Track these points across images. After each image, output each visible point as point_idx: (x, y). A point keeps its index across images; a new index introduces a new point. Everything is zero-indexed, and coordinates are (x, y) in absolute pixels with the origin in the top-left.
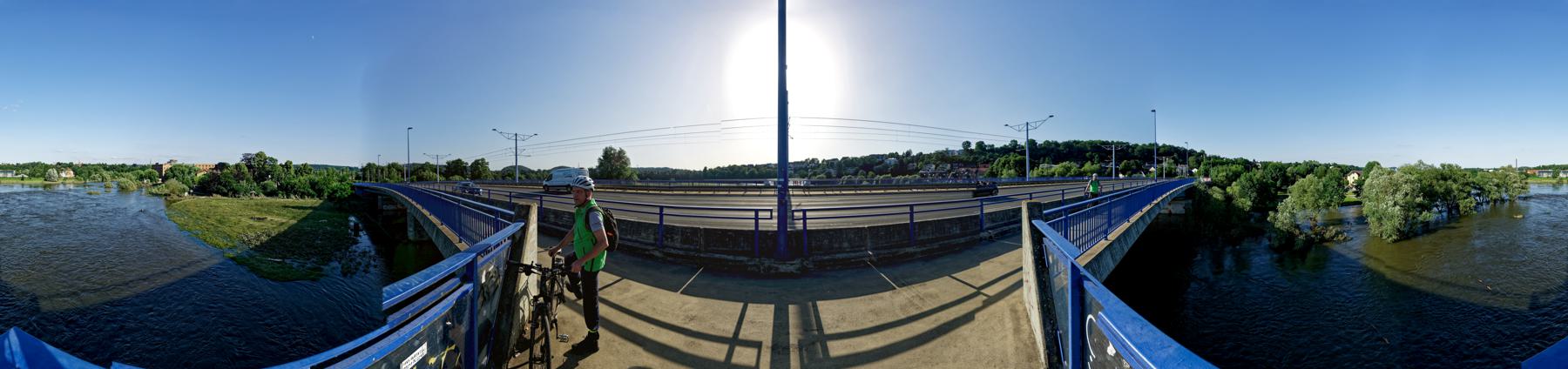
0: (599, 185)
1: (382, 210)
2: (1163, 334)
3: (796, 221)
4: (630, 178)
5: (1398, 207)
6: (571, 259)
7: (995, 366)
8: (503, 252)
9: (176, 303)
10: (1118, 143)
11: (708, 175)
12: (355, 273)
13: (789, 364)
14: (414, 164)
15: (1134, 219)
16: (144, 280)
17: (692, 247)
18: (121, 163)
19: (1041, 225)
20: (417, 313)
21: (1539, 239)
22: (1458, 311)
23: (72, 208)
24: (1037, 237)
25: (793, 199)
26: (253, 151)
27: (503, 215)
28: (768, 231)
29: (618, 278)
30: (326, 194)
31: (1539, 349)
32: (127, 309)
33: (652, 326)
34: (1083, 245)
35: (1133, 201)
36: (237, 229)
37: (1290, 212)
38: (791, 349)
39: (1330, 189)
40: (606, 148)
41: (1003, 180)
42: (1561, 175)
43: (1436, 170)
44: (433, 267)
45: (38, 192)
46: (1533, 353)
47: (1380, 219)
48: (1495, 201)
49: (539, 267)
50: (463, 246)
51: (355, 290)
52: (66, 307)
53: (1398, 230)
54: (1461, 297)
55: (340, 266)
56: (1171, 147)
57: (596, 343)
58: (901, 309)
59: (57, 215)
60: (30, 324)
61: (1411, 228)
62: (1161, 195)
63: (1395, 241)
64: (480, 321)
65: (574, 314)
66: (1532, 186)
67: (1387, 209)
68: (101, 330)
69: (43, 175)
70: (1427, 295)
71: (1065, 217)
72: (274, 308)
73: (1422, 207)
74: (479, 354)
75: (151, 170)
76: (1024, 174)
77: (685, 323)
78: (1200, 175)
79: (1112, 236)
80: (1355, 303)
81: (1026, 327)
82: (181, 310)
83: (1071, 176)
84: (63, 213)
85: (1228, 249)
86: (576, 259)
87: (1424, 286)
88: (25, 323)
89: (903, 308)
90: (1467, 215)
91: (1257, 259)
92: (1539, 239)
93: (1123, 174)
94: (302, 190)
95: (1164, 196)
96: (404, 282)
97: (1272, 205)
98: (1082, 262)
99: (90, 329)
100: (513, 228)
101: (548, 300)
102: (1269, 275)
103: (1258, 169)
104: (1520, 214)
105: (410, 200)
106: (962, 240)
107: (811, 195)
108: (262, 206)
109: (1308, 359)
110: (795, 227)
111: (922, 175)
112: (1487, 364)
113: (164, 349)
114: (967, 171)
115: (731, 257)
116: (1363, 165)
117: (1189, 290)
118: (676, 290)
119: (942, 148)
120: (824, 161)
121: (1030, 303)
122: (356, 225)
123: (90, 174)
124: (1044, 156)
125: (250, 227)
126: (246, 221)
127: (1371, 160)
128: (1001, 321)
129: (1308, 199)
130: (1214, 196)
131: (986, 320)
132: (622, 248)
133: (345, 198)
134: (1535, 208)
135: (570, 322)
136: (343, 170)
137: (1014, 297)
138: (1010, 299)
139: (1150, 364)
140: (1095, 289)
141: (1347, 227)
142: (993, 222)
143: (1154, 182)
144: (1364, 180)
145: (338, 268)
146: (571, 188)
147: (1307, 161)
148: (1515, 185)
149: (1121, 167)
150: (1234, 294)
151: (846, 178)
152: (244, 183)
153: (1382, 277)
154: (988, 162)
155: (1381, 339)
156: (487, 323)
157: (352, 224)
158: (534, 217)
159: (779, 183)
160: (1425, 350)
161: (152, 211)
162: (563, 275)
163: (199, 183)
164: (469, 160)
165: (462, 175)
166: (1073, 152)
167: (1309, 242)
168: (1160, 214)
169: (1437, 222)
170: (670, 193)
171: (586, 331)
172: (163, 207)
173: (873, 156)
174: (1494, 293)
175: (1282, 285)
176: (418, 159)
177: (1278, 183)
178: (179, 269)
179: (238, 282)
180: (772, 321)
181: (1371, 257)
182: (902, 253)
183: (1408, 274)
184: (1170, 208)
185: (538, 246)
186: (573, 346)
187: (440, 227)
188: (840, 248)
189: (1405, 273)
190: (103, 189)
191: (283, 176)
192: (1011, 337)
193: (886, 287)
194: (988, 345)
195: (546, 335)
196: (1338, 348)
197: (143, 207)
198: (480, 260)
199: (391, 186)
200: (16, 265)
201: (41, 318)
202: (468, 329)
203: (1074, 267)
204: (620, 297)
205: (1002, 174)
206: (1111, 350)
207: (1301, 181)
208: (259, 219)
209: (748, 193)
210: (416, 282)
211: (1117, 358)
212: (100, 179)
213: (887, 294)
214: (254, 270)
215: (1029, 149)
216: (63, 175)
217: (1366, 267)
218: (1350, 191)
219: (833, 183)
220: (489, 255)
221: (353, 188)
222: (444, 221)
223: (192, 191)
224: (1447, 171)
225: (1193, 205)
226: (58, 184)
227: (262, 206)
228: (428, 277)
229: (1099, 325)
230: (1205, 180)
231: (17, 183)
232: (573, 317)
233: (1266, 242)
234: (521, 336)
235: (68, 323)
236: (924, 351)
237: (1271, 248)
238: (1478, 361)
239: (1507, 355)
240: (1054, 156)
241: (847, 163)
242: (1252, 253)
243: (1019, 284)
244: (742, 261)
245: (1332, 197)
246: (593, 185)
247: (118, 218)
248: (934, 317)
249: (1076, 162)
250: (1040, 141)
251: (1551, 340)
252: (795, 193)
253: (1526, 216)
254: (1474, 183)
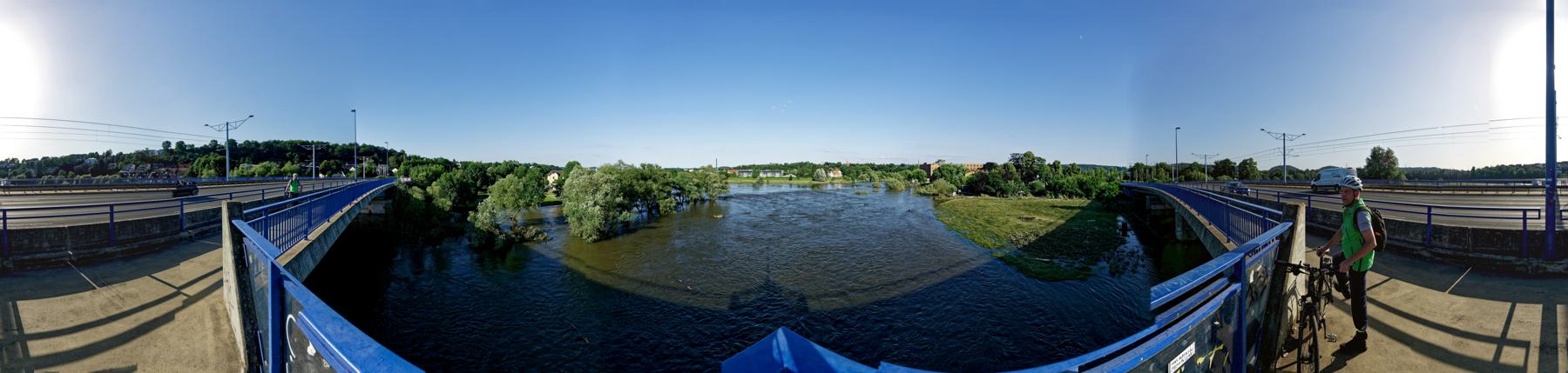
0: (1368, 185)
1: (1151, 210)
2: (364, 334)
3: (1564, 221)
4: (1398, 178)
5: (598, 207)
6: (1339, 259)
7: (195, 366)
8: (1271, 252)
9: (945, 302)
10: (318, 143)
11: (1475, 175)
12: (1123, 273)
13: (1557, 364)
14: (1182, 164)
15: (333, 219)
16: (912, 280)
17: (1460, 247)
18: (889, 163)
19: (241, 225)
20: (1185, 313)
21: (739, 239)
22: (658, 311)
23: (840, 207)
24: (237, 237)
25: (1561, 199)
26: (1021, 151)
27: (1272, 215)
28: (1536, 231)
29: (1387, 278)
30: (1094, 194)
31: (739, 349)
32: (895, 309)
33: (1421, 326)
34: (283, 245)
35: (333, 201)
36: (1006, 229)
37: (489, 212)
38: (1559, 349)
39: (530, 189)
40: (1375, 148)
41: (204, 180)
42: (761, 175)
43: (636, 170)
44: (1201, 267)
45: (806, 192)
46: (732, 353)
47: (580, 219)
48: (695, 201)
49: (1307, 267)
50: (1231, 246)
52: (834, 307)
53: (599, 230)
54: (662, 297)
55: (1108, 266)
56: (371, 147)
57: (1365, 342)
58: (102, 309)
59: (825, 215)
60: (798, 324)
61: (611, 228)
62: (361, 195)
63: (595, 241)
64: (1248, 320)
65: (1342, 313)
66: (732, 186)
67: (587, 209)
68: (868, 330)
69: (811, 175)
70: (627, 294)
71: (264, 216)
72: (1042, 308)
73: (622, 207)
74: (1247, 354)
75: (918, 170)
76: (224, 174)
77: (1452, 323)
78: (400, 175)
79: (312, 236)
80: (555, 303)
81: (226, 326)
82: (950, 310)
83: (271, 176)
84: (831, 213)
85: (429, 249)
86: (1345, 259)
87: (625, 286)
88: (793, 323)
89: (103, 308)
90: (667, 215)
91: (456, 259)
92: (739, 239)
93: (324, 174)
94: (1070, 190)
95: (364, 196)
96: (1173, 282)
97: (471, 205)
98: (282, 262)
99: (859, 328)
100: (1281, 228)
101: (1316, 300)
103: (458, 169)
104: (719, 214)
105: (1178, 200)
106: (162, 240)
107: (11, 195)
108: (1030, 205)
109: (508, 359)
110: (1563, 227)
111: (122, 175)
112: (688, 363)
113: (931, 349)
114: (167, 170)
115: (1499, 257)
116: (563, 165)
117: (389, 290)
118: (1444, 291)
119: (142, 148)
120: (24, 161)
121: (230, 303)
122: (1124, 225)
123: (858, 173)
124: (245, 156)
125: (1018, 226)
126: (1014, 221)
127: (572, 161)
128: (201, 321)
129: (508, 199)
130: (414, 196)
131: (186, 320)
132: (1390, 248)
133: (1113, 198)
134: (735, 208)
135: (1338, 322)
136: (1111, 170)
137: (214, 297)
138: (211, 299)
139: (351, 364)
140: (295, 289)
141: (547, 227)
142: (193, 221)
143: (354, 182)
144: (564, 180)
145: (1105, 267)
146: (1340, 188)
147: (507, 161)
148: (716, 185)
149: (322, 166)
150: (434, 294)
151: (46, 177)
152: (1012, 183)
153: (581, 277)
154: (188, 162)
155: (580, 339)
156: (1256, 323)
157: (1120, 224)
158: (1302, 217)
159: (1547, 183)
160: (625, 350)
161: (920, 211)
162: (1331, 275)
163: (968, 183)
164: (1237, 160)
165: (1230, 175)
166: (274, 152)
167: (510, 242)
168: (360, 214)
169: (637, 222)
170: (1438, 192)
171: (1353, 331)
172: (931, 207)
173: (73, 156)
174: (694, 293)
175: (482, 285)
176: (1187, 159)
177: (479, 183)
178: (947, 269)
179: (1005, 282)
180: (1540, 321)
181: (571, 257)
182: (103, 252)
183: (609, 274)
184: (370, 207)
185: (1307, 246)
186: (1341, 346)
187: (1208, 227)
188: (40, 248)
189: (605, 272)
190: (871, 189)
191: (1051, 176)
192: (211, 337)
193: (87, 287)
194: (187, 345)
195: (1314, 335)
196: (538, 347)
197: (911, 207)
198: (1248, 260)
199: (1159, 186)
200: (784, 265)
201: (809, 318)
202: (1236, 328)
203: (274, 267)
204: (1389, 297)
205: (202, 174)
206: (311, 350)
207: (501, 181)
208: (1027, 219)
209: (1516, 193)
210: (1184, 282)
211: (317, 358)
212: (868, 179)
213: (88, 293)
214: (1021, 269)
215: (229, 149)
216: (831, 175)
217: (567, 267)
218: (550, 191)
219: (34, 182)
220: (1257, 255)
221: (1121, 187)
222: (1212, 220)
223: (960, 191)
224: (647, 171)
225: (392, 205)
226: (826, 184)
227: (1030, 205)
228: (1196, 276)
229: (298, 323)
230: (406, 180)
231: (785, 183)
232: (1342, 317)
233: (466, 242)
234: (1289, 336)
235: (836, 323)
236: (125, 351)
237: (471, 247)
238: (678, 361)
239: (707, 355)
240: (254, 156)
241: (48, 163)
242: (452, 252)
243: (219, 284)
244: (1510, 261)
245: (532, 197)
246: (1361, 185)
247: (886, 218)
248: (133, 317)
249: (276, 161)
250: (240, 141)
251: (750, 340)
252: (1563, 193)
253: (727, 216)
254: (674, 183)
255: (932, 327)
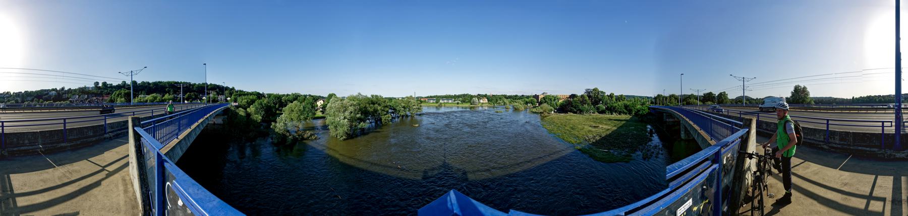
0: (792, 107)
1: (666, 121)
2: (211, 193)
3: (906, 128)
4: (809, 103)
5: (346, 120)
6: (775, 150)
7: (113, 212)
8: (736, 146)
9: (547, 175)
10: (184, 83)
11: (854, 101)
12: (650, 158)
13: (902, 211)
14: (684, 95)
15: (193, 127)
16: (528, 162)
17: (845, 143)
18: (515, 94)
19: (140, 130)
20: (686, 181)
21: (428, 138)
22: (381, 180)
23: (486, 120)
24: (137, 137)
25: (904, 115)
26: (591, 87)
27: (736, 125)
28: (889, 134)
29: (803, 161)
30: (634, 112)
31: (428, 202)
32: (518, 179)
33: (823, 189)
34: (164, 142)
35: (193, 116)
36: (582, 133)
37: (283, 123)
38: (903, 202)
39: (307, 109)
40: (796, 86)
41: (118, 104)
42: (441, 101)
43: (368, 98)
44: (695, 155)
45: (467, 111)
46: (424, 205)
47: (336, 127)
48: (403, 116)
49: (757, 155)
50: (713, 142)
51: (651, 168)
52: (483, 178)
53: (347, 133)
54: (383, 172)
55: (642, 154)
56: (215, 85)
57: (790, 198)
58: (59, 179)
59: (478, 124)
60: (462, 188)
61: (354, 132)
62: (209, 113)
63: (344, 140)
64: (723, 186)
65: (777, 181)
66: (424, 108)
67: (340, 121)
68: (503, 191)
69: (470, 101)
70: (363, 170)
71: (153, 125)
72: (603, 178)
73: (360, 120)
74: (722, 205)
75: (532, 98)
76: (130, 101)
77: (841, 187)
78: (231, 101)
79: (181, 137)
80: (321, 175)
81: (131, 189)
82: (550, 179)
83: (157, 102)
84: (481, 123)
85: (248, 144)
86: (779, 150)
87: (362, 166)
88: (459, 187)
89: (59, 178)
90: (386, 124)
91: (264, 150)
92: (428, 138)
93: (188, 101)
94: (620, 110)
95: (211, 113)
96: (679, 163)
97: (273, 119)
98: (163, 152)
99: (497, 190)
100: (742, 132)
101: (762, 173)
102: (272, 159)
103: (265, 98)
104: (417, 124)
105: (682, 116)
106: (94, 139)
107: (6, 113)
108: (596, 119)
109: (294, 208)
110: (905, 132)
111: (71, 101)
112: (398, 210)
113: (539, 202)
114: (97, 99)
115: (868, 149)
116: (326, 95)
117: (225, 168)
118: (836, 168)
119: (82, 86)
120: (14, 93)
121: (133, 175)
122: (651, 130)
123: (497, 100)
124: (142, 90)
125: (590, 131)
126: (587, 128)
127: (331, 93)
128: (117, 186)
129: (294, 115)
130: (240, 113)
131: (108, 185)
132: (805, 144)
133: (644, 114)
134: (425, 120)
135: (775, 187)
136: (643, 99)
137: (124, 172)
138: (122, 173)
139: (203, 211)
140: (171, 167)
141: (317, 132)
142: (112, 128)
143: (205, 106)
144: (327, 104)
145: (640, 154)
146: (776, 109)
147: (294, 93)
148: (414, 107)
149: (186, 96)
150: (251, 170)
151: (26, 103)
152: (586, 106)
153: (337, 160)
154: (109, 94)
155: (336, 196)
156: (727, 187)
157: (649, 129)
158: (754, 126)
159: (896, 106)
160: (362, 203)
161: (533, 122)
162: (771, 159)
163: (560, 106)
164: (716, 93)
165: (712, 101)
166: (158, 88)
167: (295, 140)
168: (208, 124)
169: (369, 129)
170: (833, 111)
171: (784, 192)
172: (539, 120)
173: (42, 90)
174: (402, 170)
175: (279, 165)
176: (687, 92)
177: (277, 106)
178: (548, 156)
179: (582, 164)
180: (892, 186)
181: (331, 149)
182: (60, 146)
183: (353, 158)
184: (214, 120)
185: (757, 142)
186: (776, 200)
187: (699, 131)
188: (23, 143)
189: (351, 158)
190: (504, 110)
191: (609, 102)
192: (122, 195)
193: (50, 166)
194: (109, 200)
195: (761, 194)
196: (312, 201)
197: (528, 120)
198: (723, 151)
199: (671, 108)
200: (454, 153)
201: (468, 184)
202: (716, 190)
203: (158, 154)
204: (804, 172)
205: (117, 101)
206: (180, 203)
207: (290, 105)
208: (595, 127)
209: (878, 112)
210: (686, 163)
211: (184, 208)
212: (503, 104)
213: (51, 170)
214: (591, 156)
215: (133, 86)
216: (481, 101)
217: (328, 154)
218: (319, 111)
219: (19, 106)
220: (728, 148)
221: (649, 109)
222: (702, 127)
223: (556, 111)
224: (374, 99)
225: (227, 118)
226: (479, 107)
227: (596, 119)
228: (693, 160)
229: (172, 187)
230: (235, 104)
231: (455, 106)
232: (777, 184)
233: (270, 140)
234: (746, 195)
235: (484, 187)
236: (72, 203)
237: (272, 143)
238: (393, 209)
239: (410, 205)
240: (147, 90)
241: (28, 94)
242: (262, 146)
243: (127, 164)
244: (874, 151)
245: (308, 114)
246: (788, 107)
247: (513, 126)
248: (77, 183)
249: (160, 93)
250: (139, 82)
251: (434, 197)
252: (905, 112)
253: (421, 125)
254: (390, 106)
255: (540, 189)
